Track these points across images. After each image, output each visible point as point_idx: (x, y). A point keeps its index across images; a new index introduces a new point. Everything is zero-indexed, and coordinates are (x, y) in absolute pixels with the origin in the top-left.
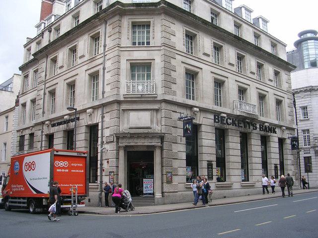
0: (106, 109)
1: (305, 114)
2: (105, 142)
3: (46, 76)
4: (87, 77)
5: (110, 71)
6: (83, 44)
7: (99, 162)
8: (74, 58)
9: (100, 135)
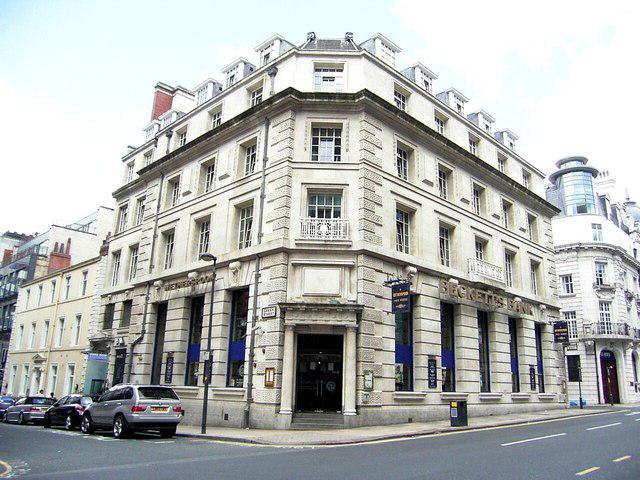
0: (265, 263)
1: (570, 288)
2: (260, 318)
3: (159, 207)
4: (232, 210)
5: (272, 201)
6: (227, 157)
7: (247, 352)
9: (251, 305)
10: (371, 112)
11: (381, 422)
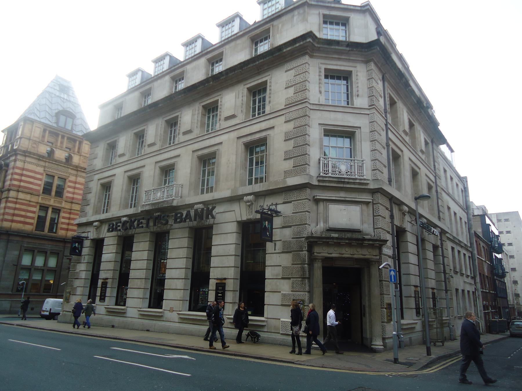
6: (232, 100)
8: (171, 134)
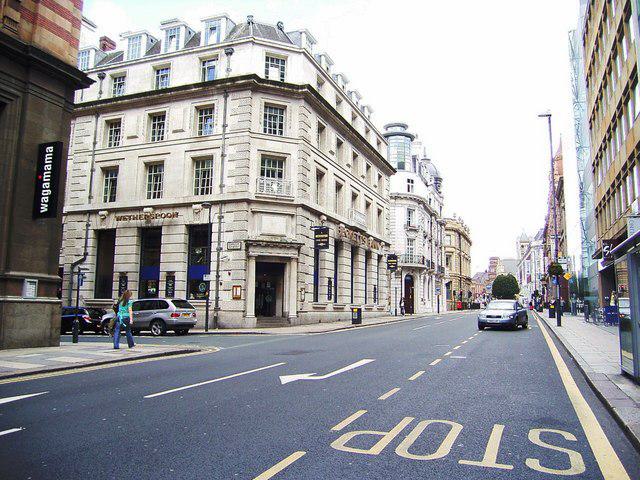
0: (226, 208)
2: (225, 248)
3: (95, 143)
10: (308, 100)
11: (306, 323)
